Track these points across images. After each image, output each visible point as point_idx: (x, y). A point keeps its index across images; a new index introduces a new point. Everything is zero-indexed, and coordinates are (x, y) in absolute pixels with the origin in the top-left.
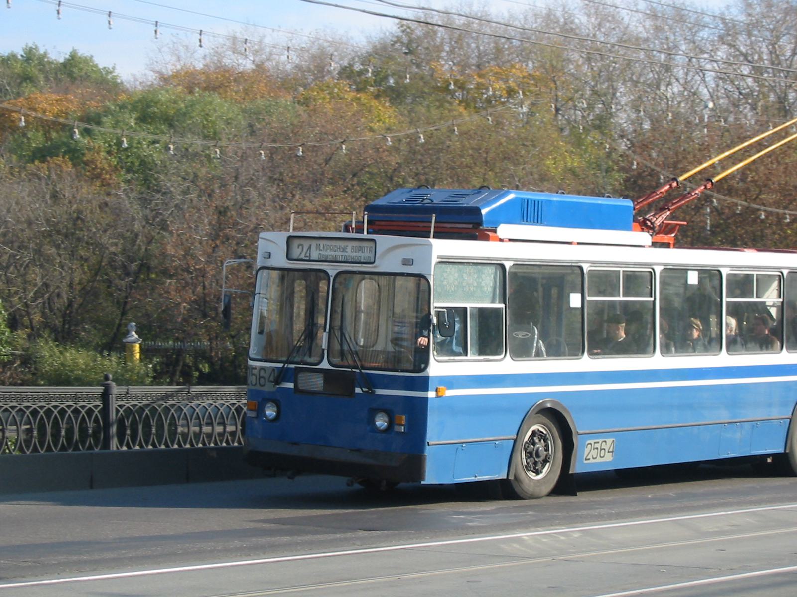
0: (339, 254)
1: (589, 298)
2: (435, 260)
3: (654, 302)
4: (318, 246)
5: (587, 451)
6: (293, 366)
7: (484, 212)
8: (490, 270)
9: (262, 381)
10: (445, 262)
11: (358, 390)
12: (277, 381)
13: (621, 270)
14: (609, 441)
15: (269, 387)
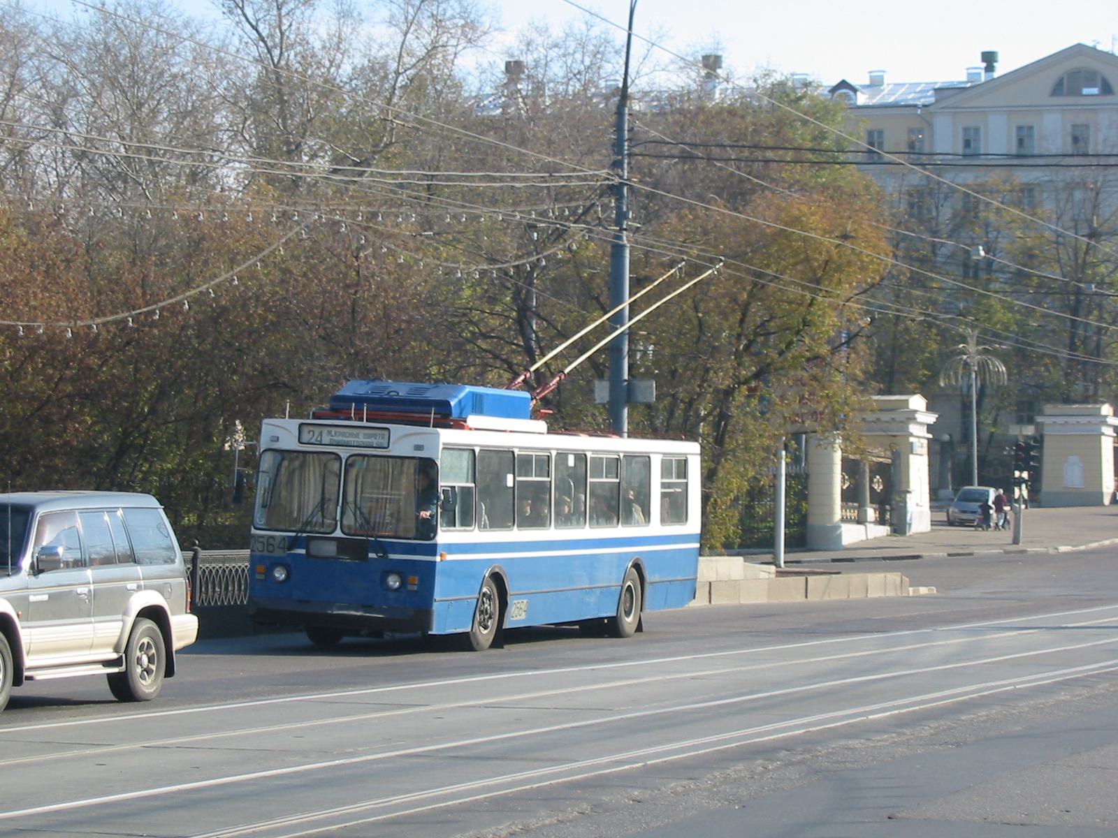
0: (352, 440)
1: (518, 479)
2: (441, 447)
3: (551, 482)
4: (330, 433)
5: (513, 609)
6: (304, 535)
7: (452, 403)
8: (466, 455)
9: (271, 548)
10: (448, 448)
11: (372, 555)
12: (290, 548)
13: (673, 459)
14: (525, 601)
15: (279, 553)
